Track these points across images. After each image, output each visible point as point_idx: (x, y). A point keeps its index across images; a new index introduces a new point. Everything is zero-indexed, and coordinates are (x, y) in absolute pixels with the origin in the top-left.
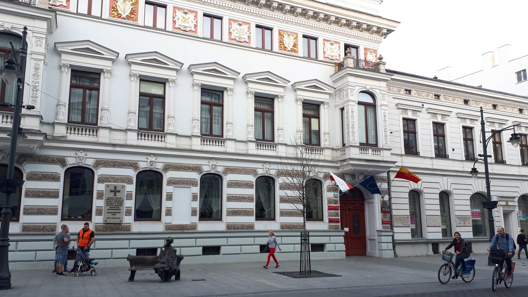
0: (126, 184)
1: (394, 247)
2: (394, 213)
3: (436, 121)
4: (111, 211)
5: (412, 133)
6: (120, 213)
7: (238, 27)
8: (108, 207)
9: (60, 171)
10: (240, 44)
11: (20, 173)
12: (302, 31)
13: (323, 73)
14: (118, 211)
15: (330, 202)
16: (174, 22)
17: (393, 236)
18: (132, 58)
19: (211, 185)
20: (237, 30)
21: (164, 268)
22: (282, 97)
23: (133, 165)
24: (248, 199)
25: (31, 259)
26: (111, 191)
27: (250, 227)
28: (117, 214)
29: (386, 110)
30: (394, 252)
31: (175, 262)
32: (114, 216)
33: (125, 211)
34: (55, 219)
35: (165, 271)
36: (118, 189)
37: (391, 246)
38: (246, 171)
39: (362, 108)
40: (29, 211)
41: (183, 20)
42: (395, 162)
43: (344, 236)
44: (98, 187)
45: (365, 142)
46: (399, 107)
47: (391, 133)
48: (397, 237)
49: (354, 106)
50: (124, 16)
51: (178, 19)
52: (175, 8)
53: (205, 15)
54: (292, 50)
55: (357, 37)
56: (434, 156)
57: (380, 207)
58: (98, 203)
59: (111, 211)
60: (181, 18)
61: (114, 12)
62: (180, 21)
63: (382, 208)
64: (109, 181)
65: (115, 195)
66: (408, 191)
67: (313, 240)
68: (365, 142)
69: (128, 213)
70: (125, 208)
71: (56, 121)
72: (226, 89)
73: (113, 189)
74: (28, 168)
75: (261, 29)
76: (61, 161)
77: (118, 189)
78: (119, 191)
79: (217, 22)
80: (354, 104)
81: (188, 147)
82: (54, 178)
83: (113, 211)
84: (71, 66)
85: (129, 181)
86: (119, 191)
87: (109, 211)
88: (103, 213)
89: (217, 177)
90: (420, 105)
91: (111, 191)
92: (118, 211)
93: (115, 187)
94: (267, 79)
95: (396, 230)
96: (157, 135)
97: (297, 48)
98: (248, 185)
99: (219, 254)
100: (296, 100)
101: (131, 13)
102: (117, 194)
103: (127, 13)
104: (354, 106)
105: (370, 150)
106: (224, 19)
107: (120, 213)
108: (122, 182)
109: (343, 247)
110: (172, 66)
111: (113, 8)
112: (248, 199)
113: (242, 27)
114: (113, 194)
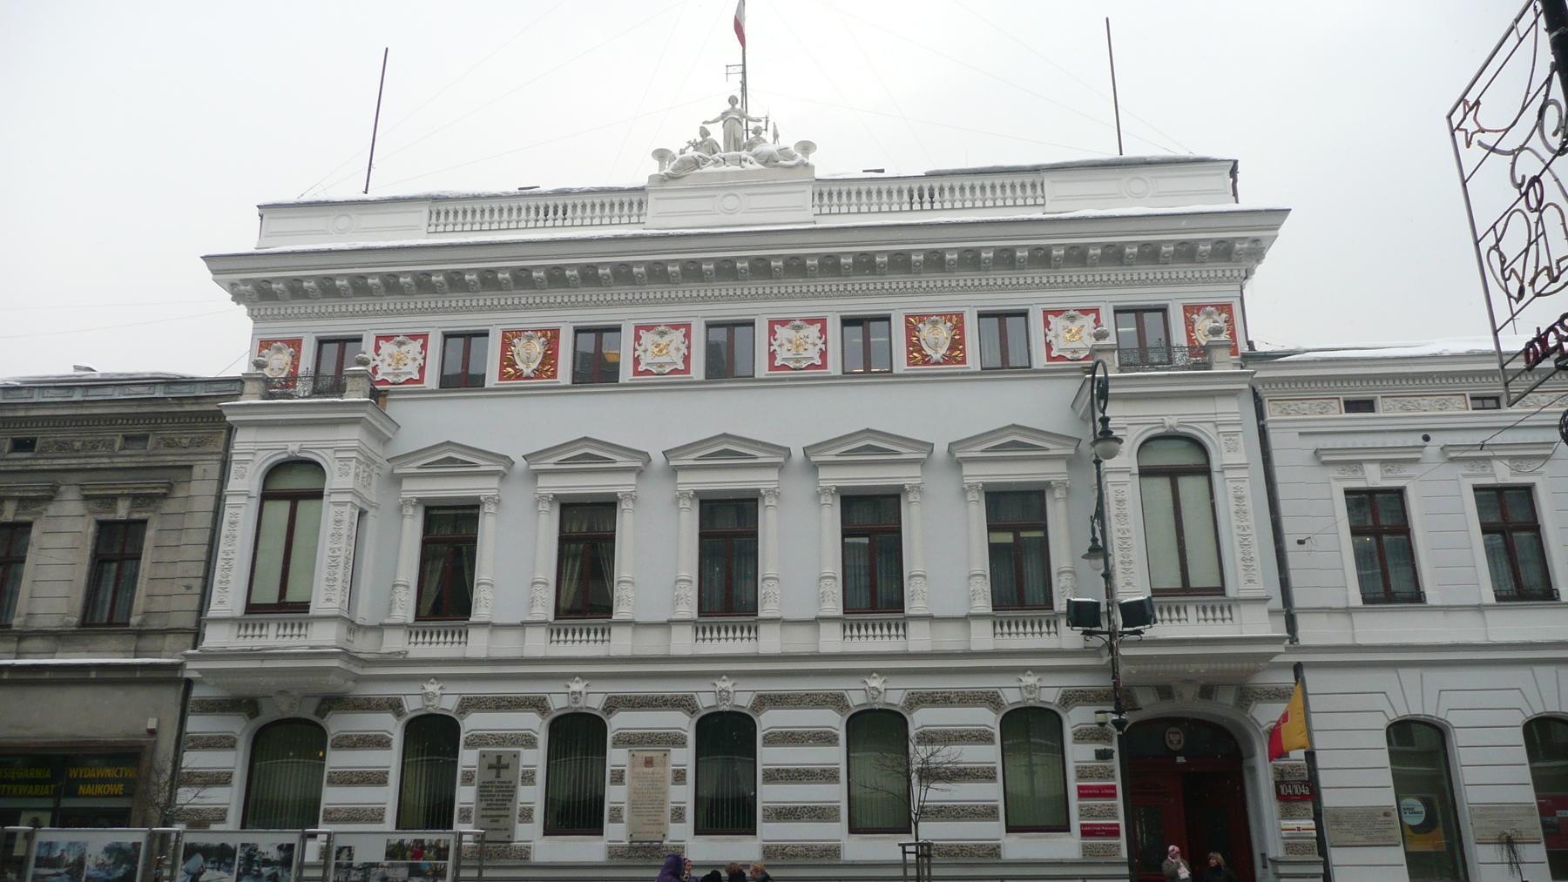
2: (1329, 800)
5: (1393, 531)
7: (657, 338)
8: (484, 804)
9: (393, 727)
10: (812, 375)
11: (322, 733)
12: (834, 310)
13: (1043, 405)
15: (1082, 773)
16: (1049, 346)
18: (400, 466)
19: (726, 736)
22: (498, 503)
23: (992, 700)
26: (490, 767)
29: (1242, 480)
32: (495, 825)
36: (503, 762)
44: (468, 758)
45: (1179, 585)
46: (1325, 458)
47: (1301, 542)
49: (1124, 483)
50: (527, 371)
51: (1056, 336)
52: (1046, 313)
54: (948, 360)
55: (1155, 283)
56: (1356, 599)
57: (1272, 783)
58: (465, 796)
60: (651, 348)
62: (1061, 339)
63: (1277, 785)
65: (498, 776)
68: (1179, 585)
69: (678, 815)
70: (519, 806)
71: (387, 621)
73: (494, 762)
74: (338, 724)
76: (395, 706)
77: (503, 762)
78: (507, 767)
81: (1348, 641)
82: (381, 743)
85: (678, 741)
86: (507, 767)
88: (625, 818)
91: (490, 767)
93: (499, 757)
94: (587, 456)
95: (1336, 855)
97: (963, 351)
100: (964, 492)
101: (952, 348)
102: (503, 772)
103: (943, 351)
104: (1124, 483)
105: (1191, 610)
106: (1031, 315)
108: (514, 744)
110: (908, 454)
111: (913, 345)
112: (773, 776)
114: (494, 772)
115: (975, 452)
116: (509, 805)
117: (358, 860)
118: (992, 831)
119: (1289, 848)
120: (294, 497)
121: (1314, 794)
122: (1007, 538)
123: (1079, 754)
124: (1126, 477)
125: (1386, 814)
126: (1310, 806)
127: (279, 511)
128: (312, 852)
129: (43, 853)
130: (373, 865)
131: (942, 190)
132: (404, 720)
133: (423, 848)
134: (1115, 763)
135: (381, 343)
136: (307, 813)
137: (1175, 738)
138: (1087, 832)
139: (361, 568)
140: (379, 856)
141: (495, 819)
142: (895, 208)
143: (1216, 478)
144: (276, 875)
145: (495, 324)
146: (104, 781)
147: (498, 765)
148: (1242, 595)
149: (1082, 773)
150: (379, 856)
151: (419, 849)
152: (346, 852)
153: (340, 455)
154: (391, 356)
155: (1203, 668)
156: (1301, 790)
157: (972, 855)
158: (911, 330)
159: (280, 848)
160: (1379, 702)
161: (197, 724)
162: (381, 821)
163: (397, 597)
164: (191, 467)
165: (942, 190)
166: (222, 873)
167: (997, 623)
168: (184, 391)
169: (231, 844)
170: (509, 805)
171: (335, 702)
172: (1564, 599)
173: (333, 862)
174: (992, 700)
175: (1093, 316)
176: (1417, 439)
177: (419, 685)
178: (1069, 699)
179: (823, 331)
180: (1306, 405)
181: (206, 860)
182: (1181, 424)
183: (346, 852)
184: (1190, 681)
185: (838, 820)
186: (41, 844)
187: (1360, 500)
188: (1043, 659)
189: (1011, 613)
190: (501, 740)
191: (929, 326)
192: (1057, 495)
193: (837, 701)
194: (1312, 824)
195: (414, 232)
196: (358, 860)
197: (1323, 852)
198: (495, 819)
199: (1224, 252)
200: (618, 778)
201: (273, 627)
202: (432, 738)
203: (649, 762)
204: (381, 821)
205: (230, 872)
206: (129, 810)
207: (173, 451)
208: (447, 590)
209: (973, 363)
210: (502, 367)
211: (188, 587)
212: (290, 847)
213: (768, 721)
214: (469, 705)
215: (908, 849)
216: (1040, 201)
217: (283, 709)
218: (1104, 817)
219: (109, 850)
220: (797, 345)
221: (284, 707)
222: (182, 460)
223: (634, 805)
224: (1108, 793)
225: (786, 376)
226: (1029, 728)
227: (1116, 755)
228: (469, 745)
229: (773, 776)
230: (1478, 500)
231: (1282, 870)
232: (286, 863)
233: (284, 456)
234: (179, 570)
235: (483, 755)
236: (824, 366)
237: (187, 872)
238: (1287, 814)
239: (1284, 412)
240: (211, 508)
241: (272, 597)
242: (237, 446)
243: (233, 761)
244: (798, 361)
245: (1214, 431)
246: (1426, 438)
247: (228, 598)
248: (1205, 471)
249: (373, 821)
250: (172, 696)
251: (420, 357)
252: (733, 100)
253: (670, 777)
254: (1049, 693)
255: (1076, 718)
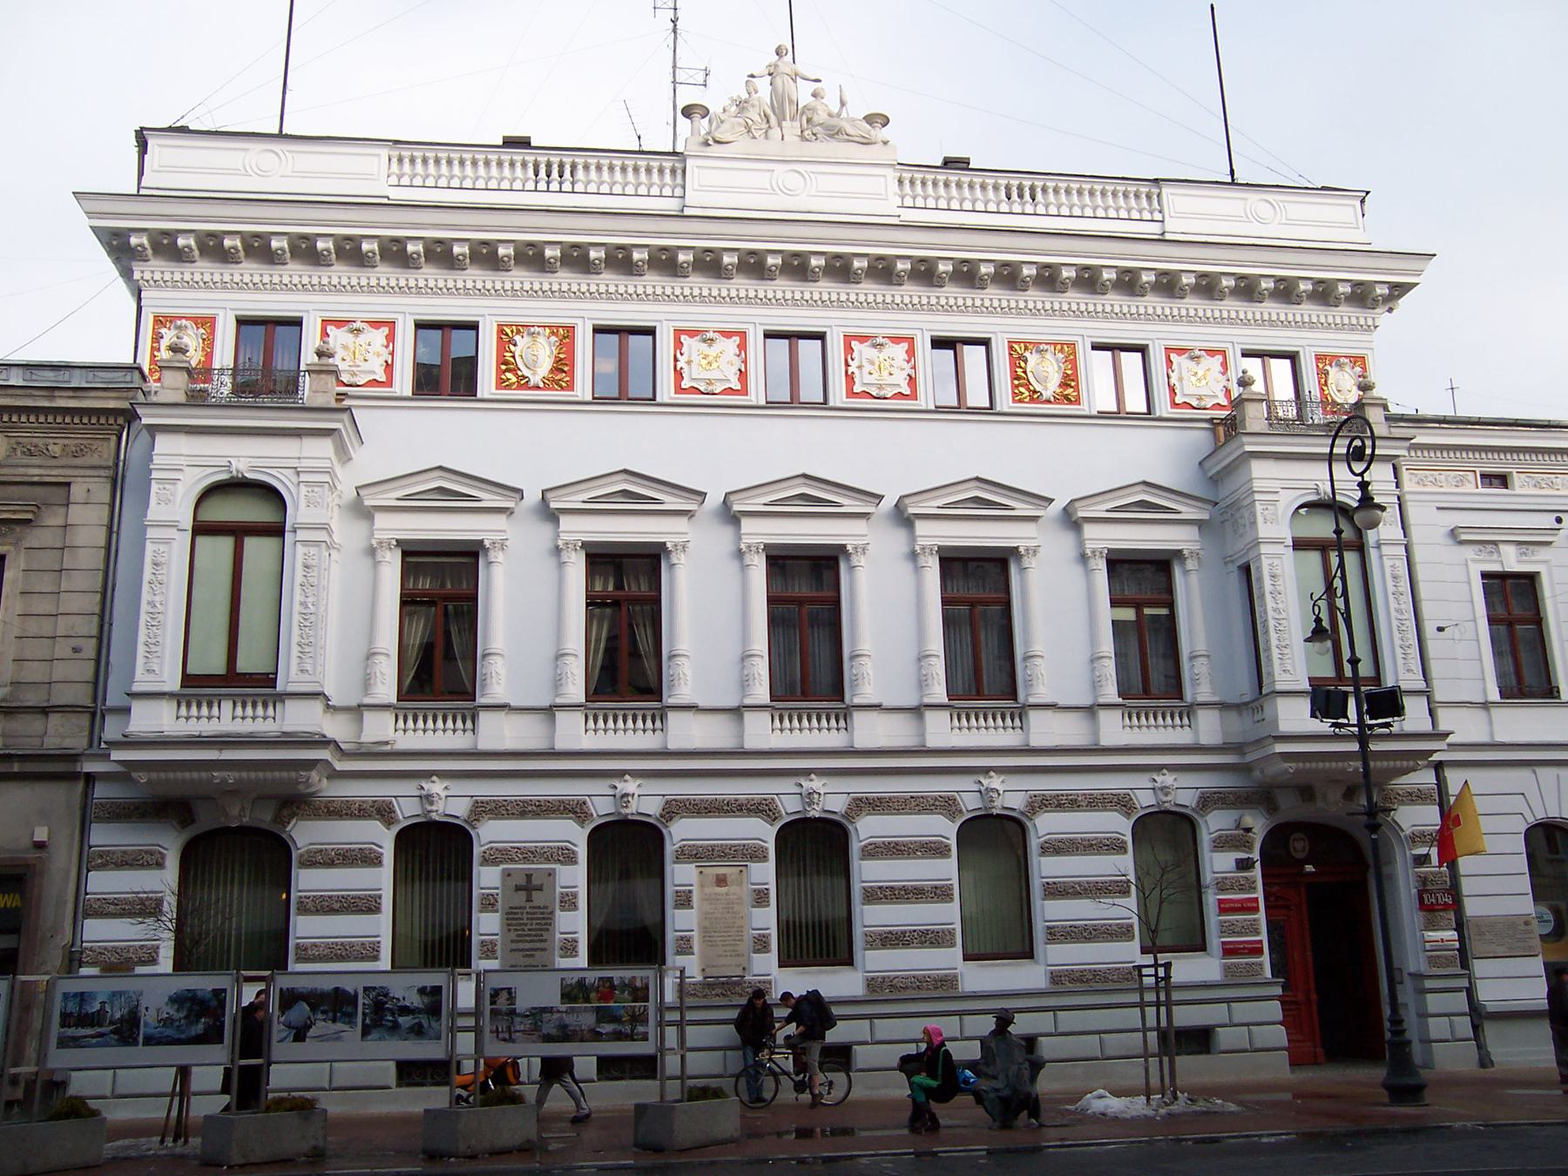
0: (557, 866)
1: (1476, 1028)
2: (1472, 908)
3: (1496, 568)
4: (521, 946)
6: (544, 950)
9: (384, 839)
11: (282, 849)
12: (757, 320)
14: (538, 945)
17: (1470, 992)
19: (815, 846)
20: (872, 363)
21: (996, 1090)
23: (575, 810)
24: (1056, 891)
25: (1090, 1054)
26: (518, 888)
27: (944, 985)
28: (537, 954)
30: (1479, 1047)
31: (1026, 1074)
32: (529, 961)
33: (557, 945)
34: (1129, 952)
35: (1000, 1098)
36: (536, 882)
37: (1464, 1025)
38: (1096, 802)
39: (1314, 557)
40: (1058, 935)
41: (704, 362)
42: (1447, 735)
43: (1279, 998)
44: (486, 878)
46: (1464, 537)
47: (1440, 629)
48: (1491, 994)
50: (1047, 394)
53: (769, 335)
56: (1494, 695)
57: (1414, 891)
58: (487, 925)
59: (521, 946)
61: (509, 375)
64: (512, 860)
65: (529, 900)
66: (1523, 827)
67: (1186, 1017)
69: (761, 944)
70: (558, 936)
72: (1014, 551)
73: (523, 882)
74: (305, 834)
75: (1259, 360)
77: (536, 882)
78: (540, 889)
79: (808, 349)
80: (1279, 549)
81: (1485, 739)
82: (369, 859)
83: (528, 946)
84: (585, 545)
87: (514, 946)
88: (499, 953)
89: (1008, 824)
90: (1548, 521)
91: (518, 888)
92: (538, 945)
95: (1480, 967)
96: (649, 713)
97: (1077, 388)
98: (935, 850)
99: (1208, 1052)
104: (1279, 556)
107: (544, 950)
108: (548, 860)
109: (1279, 1035)
111: (506, 363)
112: (876, 895)
113: (362, 339)
114: (523, 894)
115: (1099, 510)
116: (546, 935)
117: (522, 1004)
118: (948, 959)
119: (1433, 961)
120: (240, 532)
121: (1457, 905)
122: (1128, 614)
123: (1218, 863)
124: (173, 533)
125: (1527, 923)
126: (1451, 915)
127: (218, 550)
128: (466, 995)
129: (72, 1007)
130: (544, 1010)
131: (574, 167)
132: (396, 829)
133: (613, 987)
134: (1257, 872)
135: (1219, 358)
136: (271, 949)
137: (1299, 845)
138: (1229, 951)
139: (340, 626)
140: (552, 998)
141: (529, 953)
142: (655, 191)
143: (1373, 554)
144: (420, 1025)
145: (489, 313)
146: (240, 903)
147: (528, 886)
148: (291, 688)
149: (1222, 886)
150: (552, 998)
151: (608, 989)
152: (504, 995)
153: (303, 477)
154: (345, 347)
155: (231, 777)
156: (1443, 900)
157: (1106, 980)
158: (1017, 360)
159: (422, 991)
160: (1518, 804)
161: (103, 836)
162: (376, 958)
163: (378, 669)
164: (68, 484)
165: (574, 167)
166: (339, 1026)
167: (958, 714)
168: (47, 379)
169: (350, 989)
170: (546, 935)
171: (297, 803)
172: (1564, 697)
173: (488, 1007)
174: (1122, 803)
175: (385, 330)
176: (1548, 521)
177: (975, 778)
178: (1208, 801)
179: (391, 338)
180: (1442, 477)
181: (314, 1008)
182: (253, 469)
183: (504, 995)
184: (1337, 781)
185: (953, 945)
186: (66, 996)
187: (1497, 583)
188: (1169, 756)
189: (1163, 702)
190: (529, 854)
191: (527, 339)
192: (1190, 564)
193: (947, 805)
194: (1453, 935)
195: (369, 175)
196: (522, 1004)
197: (1465, 964)
198: (529, 953)
199: (1362, 296)
200: (684, 901)
201: (227, 706)
202: (436, 852)
203: (721, 881)
204: (376, 958)
205: (352, 1023)
206: (16, 950)
207: (34, 461)
208: (627, 663)
209: (583, 390)
210: (500, 372)
211: (76, 650)
212: (437, 990)
213: (867, 829)
214: (864, 805)
215: (1145, 971)
216: (1158, 216)
217: (238, 815)
218: (1246, 934)
219: (178, 1000)
220: (713, 364)
221: (235, 811)
222: (55, 475)
223: (706, 932)
224: (1249, 907)
225: (698, 401)
226: (1167, 833)
227: (1258, 865)
228: (486, 861)
229: (876, 895)
230: (1487, 590)
231: (1429, 984)
232: (434, 1010)
233: (224, 476)
234: (63, 626)
235: (507, 874)
236: (389, 383)
237: (289, 1026)
238: (1431, 925)
239: (1420, 482)
240: (102, 543)
241: (217, 665)
242: (156, 460)
243: (164, 881)
244: (880, 387)
245: (294, 479)
246: (1559, 520)
247: (157, 665)
248: (276, 530)
249: (363, 959)
250: (62, 796)
251: (907, 367)
252: (779, 52)
253: (748, 898)
254: (1184, 792)
255: (1214, 823)
